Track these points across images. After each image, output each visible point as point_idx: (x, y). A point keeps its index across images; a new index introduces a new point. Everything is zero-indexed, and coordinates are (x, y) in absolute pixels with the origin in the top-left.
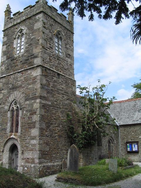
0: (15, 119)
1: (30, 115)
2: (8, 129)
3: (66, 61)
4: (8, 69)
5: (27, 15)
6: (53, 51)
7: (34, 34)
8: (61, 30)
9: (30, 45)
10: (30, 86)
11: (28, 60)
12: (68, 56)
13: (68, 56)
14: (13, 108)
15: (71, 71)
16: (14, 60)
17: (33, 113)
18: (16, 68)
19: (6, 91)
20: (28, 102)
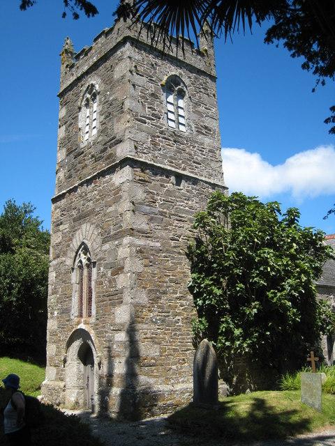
0: (85, 290)
1: (113, 274)
2: (73, 311)
3: (197, 142)
4: (70, 177)
5: (100, 53)
6: (162, 124)
8: (181, 74)
9: (107, 117)
10: (110, 209)
11: (104, 150)
12: (204, 131)
13: (204, 131)
14: (81, 261)
15: (212, 165)
16: (80, 154)
17: (118, 270)
18: (85, 171)
19: (66, 226)
20: (107, 246)
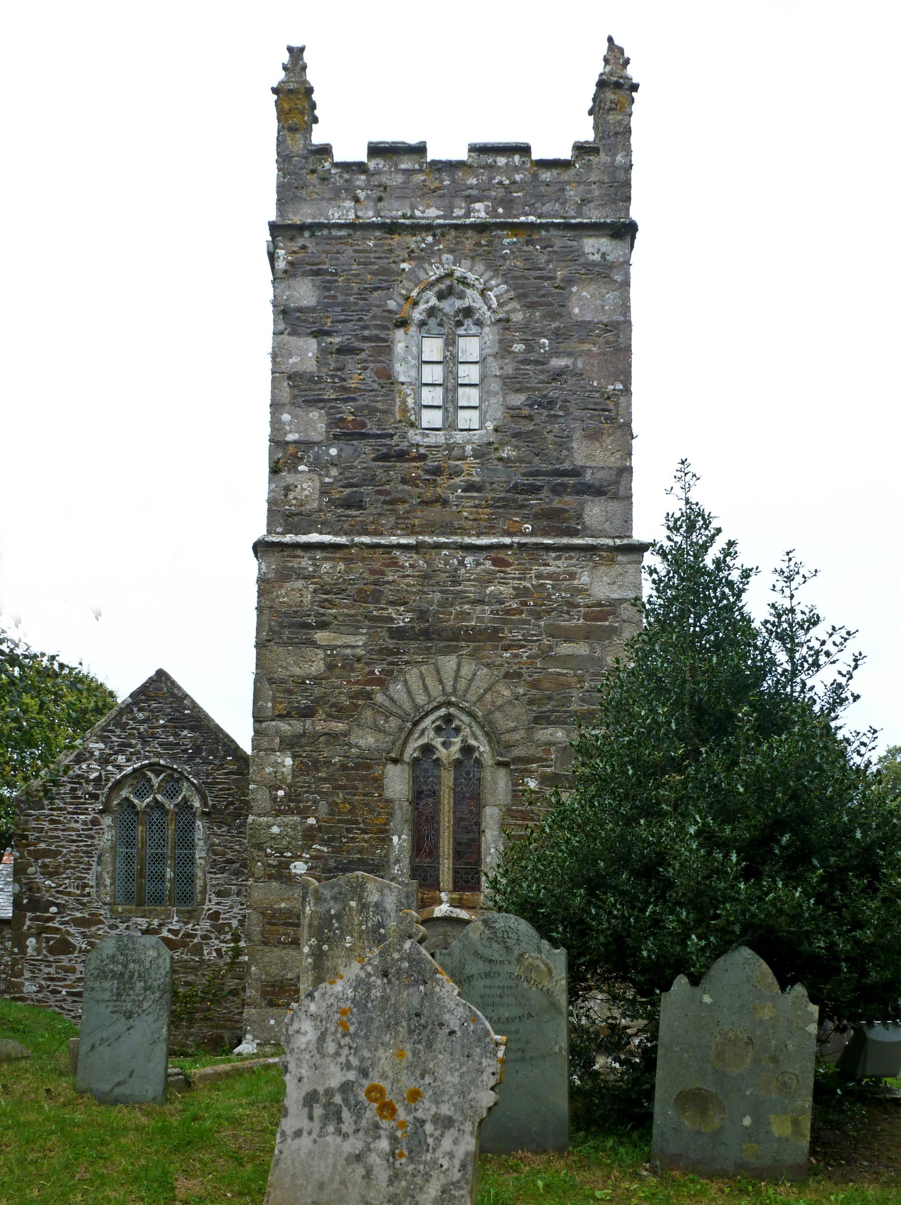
7: (572, 345)
10: (565, 648)
